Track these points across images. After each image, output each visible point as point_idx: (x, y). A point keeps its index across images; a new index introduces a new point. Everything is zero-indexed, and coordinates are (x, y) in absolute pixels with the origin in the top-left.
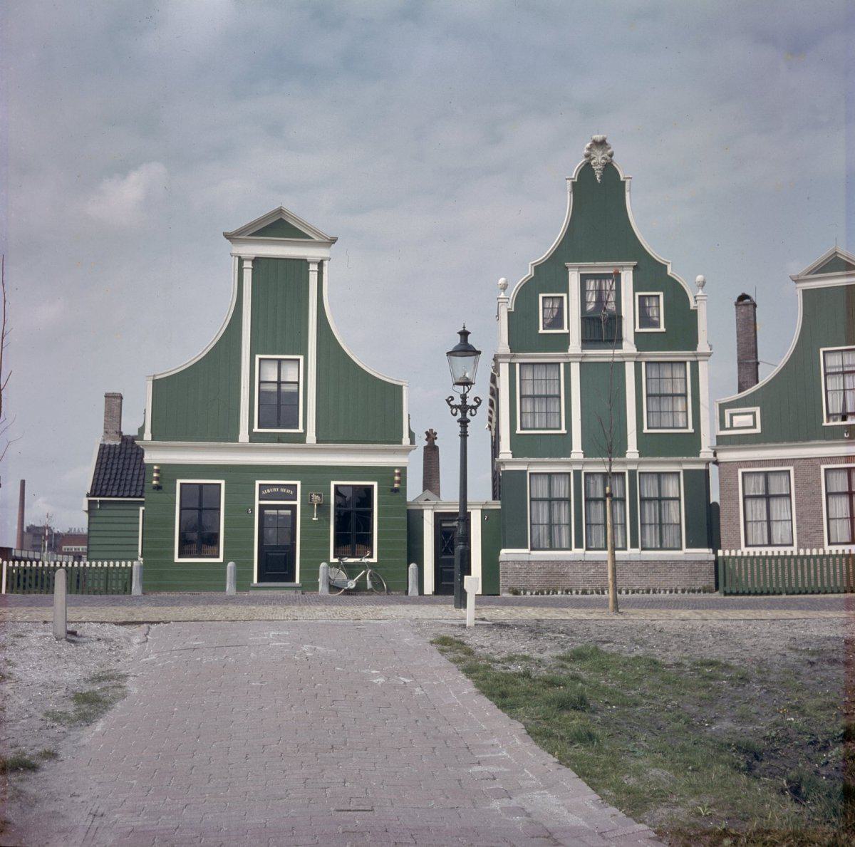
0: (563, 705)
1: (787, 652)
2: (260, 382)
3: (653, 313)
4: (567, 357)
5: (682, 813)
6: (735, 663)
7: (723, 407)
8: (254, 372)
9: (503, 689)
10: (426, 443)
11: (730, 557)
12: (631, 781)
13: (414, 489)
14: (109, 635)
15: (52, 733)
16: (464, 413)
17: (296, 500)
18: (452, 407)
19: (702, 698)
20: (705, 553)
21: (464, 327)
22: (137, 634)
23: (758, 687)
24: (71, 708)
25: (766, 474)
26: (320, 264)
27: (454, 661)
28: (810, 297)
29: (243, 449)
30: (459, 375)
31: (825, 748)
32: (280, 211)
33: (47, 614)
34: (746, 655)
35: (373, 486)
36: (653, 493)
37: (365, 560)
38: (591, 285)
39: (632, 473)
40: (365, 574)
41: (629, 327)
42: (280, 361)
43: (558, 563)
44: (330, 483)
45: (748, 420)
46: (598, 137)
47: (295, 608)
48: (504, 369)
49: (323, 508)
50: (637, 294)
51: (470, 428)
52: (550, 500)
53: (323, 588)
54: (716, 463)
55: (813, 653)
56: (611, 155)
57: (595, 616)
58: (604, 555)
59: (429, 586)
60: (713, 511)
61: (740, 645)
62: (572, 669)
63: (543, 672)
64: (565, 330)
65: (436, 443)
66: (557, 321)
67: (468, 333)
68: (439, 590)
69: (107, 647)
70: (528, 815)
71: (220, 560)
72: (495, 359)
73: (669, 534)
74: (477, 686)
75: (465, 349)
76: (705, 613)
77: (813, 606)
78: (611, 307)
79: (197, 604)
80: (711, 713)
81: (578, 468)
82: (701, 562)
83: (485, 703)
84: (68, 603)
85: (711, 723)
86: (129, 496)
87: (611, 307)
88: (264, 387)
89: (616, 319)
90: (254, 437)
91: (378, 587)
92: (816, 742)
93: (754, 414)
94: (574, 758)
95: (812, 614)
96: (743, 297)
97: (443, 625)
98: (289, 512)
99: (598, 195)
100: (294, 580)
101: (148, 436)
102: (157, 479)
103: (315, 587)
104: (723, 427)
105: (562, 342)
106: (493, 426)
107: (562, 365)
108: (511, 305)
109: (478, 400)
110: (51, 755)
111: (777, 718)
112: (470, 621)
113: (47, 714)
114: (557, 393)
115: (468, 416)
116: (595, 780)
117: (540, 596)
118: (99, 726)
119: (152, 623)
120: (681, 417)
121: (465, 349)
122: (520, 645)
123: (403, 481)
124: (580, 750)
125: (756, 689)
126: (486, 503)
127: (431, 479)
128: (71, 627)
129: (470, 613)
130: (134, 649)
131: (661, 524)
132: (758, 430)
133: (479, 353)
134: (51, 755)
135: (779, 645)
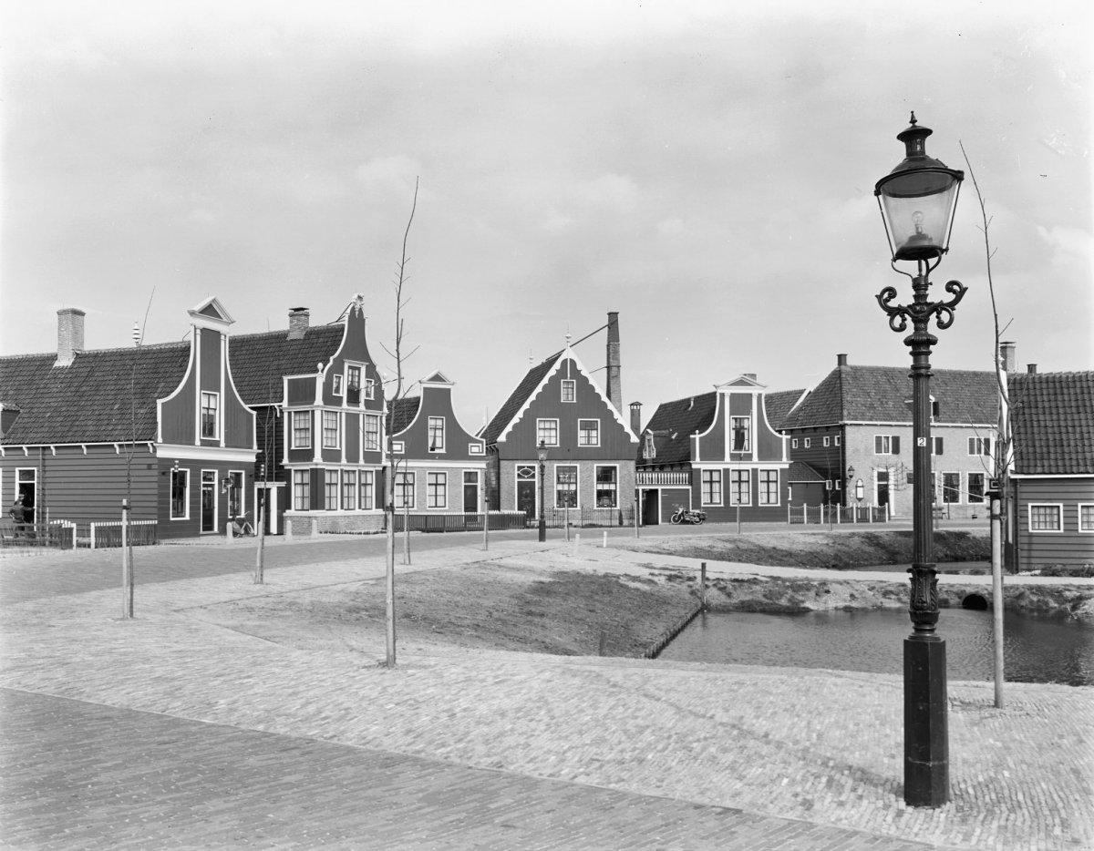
16: (920, 321)
18: (892, 312)
21: (913, 121)
30: (906, 233)
41: (363, 397)
52: (404, 485)
67: (928, 132)
109: (956, 287)
114: (334, 427)
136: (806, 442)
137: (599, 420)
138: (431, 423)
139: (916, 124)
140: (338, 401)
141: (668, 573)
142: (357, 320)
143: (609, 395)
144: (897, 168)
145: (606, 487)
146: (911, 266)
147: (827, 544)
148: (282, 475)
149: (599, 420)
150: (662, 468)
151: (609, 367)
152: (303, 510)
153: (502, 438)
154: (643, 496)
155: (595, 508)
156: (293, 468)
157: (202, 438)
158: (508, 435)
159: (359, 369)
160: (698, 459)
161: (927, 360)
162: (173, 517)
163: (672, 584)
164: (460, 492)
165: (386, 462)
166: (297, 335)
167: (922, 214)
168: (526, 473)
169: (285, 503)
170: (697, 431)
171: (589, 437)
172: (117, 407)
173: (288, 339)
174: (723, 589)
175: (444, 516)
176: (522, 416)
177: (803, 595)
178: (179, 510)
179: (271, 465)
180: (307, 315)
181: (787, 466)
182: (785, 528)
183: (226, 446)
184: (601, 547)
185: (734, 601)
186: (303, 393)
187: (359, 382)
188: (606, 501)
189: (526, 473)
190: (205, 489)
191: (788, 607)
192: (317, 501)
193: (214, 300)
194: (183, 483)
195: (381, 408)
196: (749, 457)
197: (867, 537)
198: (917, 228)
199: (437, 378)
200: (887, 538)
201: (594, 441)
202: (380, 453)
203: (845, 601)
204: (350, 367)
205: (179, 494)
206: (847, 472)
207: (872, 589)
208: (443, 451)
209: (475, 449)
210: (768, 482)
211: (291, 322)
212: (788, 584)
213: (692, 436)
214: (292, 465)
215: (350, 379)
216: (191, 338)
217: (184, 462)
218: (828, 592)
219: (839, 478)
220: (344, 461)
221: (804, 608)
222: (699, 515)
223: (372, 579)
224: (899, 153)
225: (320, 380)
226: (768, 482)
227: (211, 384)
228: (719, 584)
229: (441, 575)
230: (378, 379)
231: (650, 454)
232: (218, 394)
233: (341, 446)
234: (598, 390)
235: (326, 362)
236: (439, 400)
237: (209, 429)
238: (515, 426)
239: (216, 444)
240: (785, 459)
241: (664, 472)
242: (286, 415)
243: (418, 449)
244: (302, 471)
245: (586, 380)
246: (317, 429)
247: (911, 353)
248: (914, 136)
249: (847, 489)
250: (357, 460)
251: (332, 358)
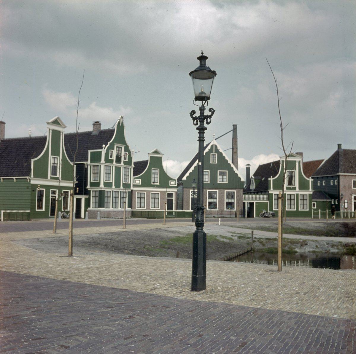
18: (194, 119)
21: (202, 53)
25: (141, 193)
29: (49, 181)
41: (123, 160)
44: (50, 190)
67: (207, 58)
87: (120, 154)
104: (134, 183)
114: (110, 172)
132: (140, 184)
136: (318, 183)
138: (153, 171)
139: (203, 55)
140: (112, 161)
141: (239, 235)
142: (121, 127)
143: (233, 162)
144: (197, 69)
145: (230, 201)
146: (199, 103)
147: (324, 227)
148: (87, 193)
150: (257, 193)
151: (233, 148)
152: (95, 208)
153: (184, 178)
154: (352, 223)
155: (225, 210)
156: (92, 190)
157: (51, 176)
158: (187, 177)
159: (121, 148)
160: (272, 189)
161: (203, 135)
162: (37, 209)
163: (240, 240)
165: (132, 188)
166: (96, 133)
167: (203, 85)
169: (88, 204)
170: (272, 177)
171: (222, 178)
172: (16, 162)
173: (92, 135)
174: (261, 242)
175: (156, 212)
177: (295, 246)
178: (40, 207)
179: (81, 187)
180: (100, 125)
181: (312, 193)
182: (310, 220)
184: (218, 225)
185: (266, 248)
186: (96, 158)
187: (121, 153)
188: (230, 206)
190: (52, 198)
191: (287, 250)
192: (101, 204)
193: (58, 118)
194: (42, 196)
195: (131, 165)
196: (295, 188)
197: (343, 224)
198: (202, 90)
199: (156, 152)
200: (351, 225)
201: (225, 180)
202: (130, 184)
203: (313, 248)
204: (117, 147)
205: (40, 200)
206: (340, 196)
207: (328, 244)
208: (158, 184)
209: (172, 183)
210: (303, 200)
211: (93, 127)
212: (289, 241)
213: (269, 179)
214: (92, 189)
215: (117, 152)
216: (47, 134)
217: (42, 186)
218: (306, 244)
219: (337, 199)
220: (114, 187)
221: (294, 251)
222: (272, 214)
223: (104, 233)
224: (197, 64)
225: (104, 152)
226: (303, 200)
227: (55, 152)
228: (260, 241)
229: (136, 233)
230: (129, 152)
231: (253, 187)
232: (59, 157)
233: (112, 181)
234: (227, 158)
235: (106, 145)
236: (157, 161)
237: (54, 172)
238: (190, 173)
240: (310, 190)
241: (262, 195)
242: (89, 167)
243: (146, 183)
244: (95, 191)
245: (221, 154)
246: (102, 173)
247: (198, 133)
248: (203, 58)
249: (340, 204)
250: (119, 187)
251: (109, 143)
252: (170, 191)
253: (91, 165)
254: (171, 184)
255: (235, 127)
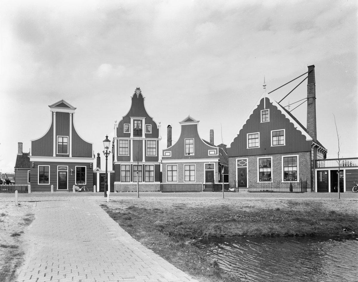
0: (126, 219)
1: (172, 206)
2: (58, 142)
3: (149, 129)
4: (130, 138)
5: (146, 240)
6: (161, 209)
7: (163, 151)
8: (58, 140)
9: (115, 216)
10: (97, 156)
11: (163, 184)
12: (138, 234)
13: (95, 167)
14: (27, 205)
15: (21, 227)
16: (107, 154)
17: (67, 170)
18: (104, 153)
19: (154, 217)
20: (159, 183)
22: (34, 204)
23: (165, 214)
24: (23, 222)
26: (72, 114)
27: (105, 210)
28: (183, 127)
31: (177, 226)
32: (62, 101)
33: (12, 199)
34: (164, 207)
35: (85, 167)
36: (148, 169)
37: (83, 184)
38: (136, 122)
39: (144, 165)
40: (83, 188)
42: (63, 137)
43: (127, 185)
44: (57, 166)
45: (169, 154)
46: (138, 88)
47: (69, 197)
48: (116, 141)
49: (73, 172)
50: (146, 125)
51: (108, 158)
53: (74, 191)
54: (162, 163)
55: (177, 207)
56: (141, 92)
57: (134, 199)
58: (136, 183)
59: (98, 190)
60: (161, 174)
61: (162, 205)
62: (129, 211)
63: (123, 212)
64: (130, 132)
65: (100, 156)
66: (128, 130)
68: (100, 191)
69: (28, 207)
70: (119, 241)
71: (49, 184)
72: (114, 138)
73: (151, 179)
74: (109, 215)
75: (107, 140)
76: (157, 198)
77: (179, 196)
78: (140, 127)
79: (46, 196)
80: (155, 219)
81: (132, 164)
82: (158, 185)
83: (111, 219)
84: (18, 196)
85: (155, 221)
86: (25, 168)
88: (59, 143)
89: (141, 130)
90: (57, 156)
91: (87, 191)
92: (175, 225)
93: (170, 153)
94: (128, 230)
95: (178, 198)
96: (169, 126)
97: (102, 201)
98: (65, 173)
99: (138, 101)
100: (67, 189)
101: (31, 155)
102: (33, 165)
103: (72, 190)
104: (163, 155)
105: (129, 135)
106: (113, 153)
107: (129, 140)
108: (117, 126)
110: (22, 232)
111: (168, 220)
112: (108, 201)
113: (18, 223)
115: (108, 155)
116: (132, 234)
117: (123, 193)
118: (31, 226)
119: (37, 201)
120: (155, 153)
121: (107, 140)
122: (118, 206)
123: (92, 166)
124: (129, 228)
125: (165, 214)
126: (111, 171)
127: (99, 165)
128: (19, 203)
129: (108, 199)
130: (34, 208)
131: (149, 176)
133: (110, 141)
134: (22, 232)
135: (170, 205)
137: (49, 166)
145: (265, 170)
149: (49, 166)
159: (142, 121)
164: (203, 174)
168: (243, 163)
176: (297, 129)
183: (72, 157)
189: (243, 163)
208: (194, 154)
224: (105, 138)
239: (68, 156)
252: (208, 162)
253: (146, 140)
254: (210, 153)
255: (311, 69)
